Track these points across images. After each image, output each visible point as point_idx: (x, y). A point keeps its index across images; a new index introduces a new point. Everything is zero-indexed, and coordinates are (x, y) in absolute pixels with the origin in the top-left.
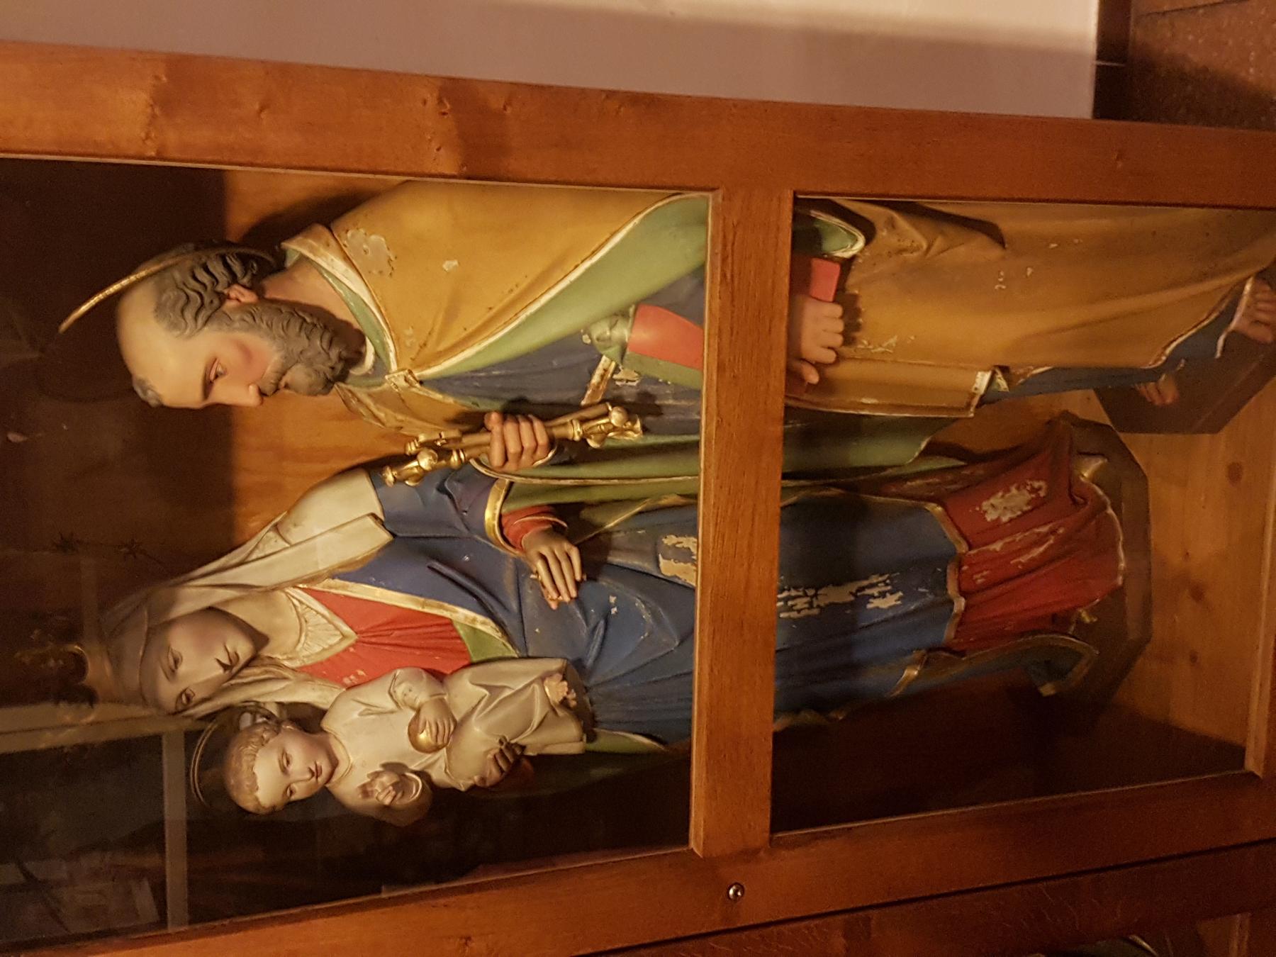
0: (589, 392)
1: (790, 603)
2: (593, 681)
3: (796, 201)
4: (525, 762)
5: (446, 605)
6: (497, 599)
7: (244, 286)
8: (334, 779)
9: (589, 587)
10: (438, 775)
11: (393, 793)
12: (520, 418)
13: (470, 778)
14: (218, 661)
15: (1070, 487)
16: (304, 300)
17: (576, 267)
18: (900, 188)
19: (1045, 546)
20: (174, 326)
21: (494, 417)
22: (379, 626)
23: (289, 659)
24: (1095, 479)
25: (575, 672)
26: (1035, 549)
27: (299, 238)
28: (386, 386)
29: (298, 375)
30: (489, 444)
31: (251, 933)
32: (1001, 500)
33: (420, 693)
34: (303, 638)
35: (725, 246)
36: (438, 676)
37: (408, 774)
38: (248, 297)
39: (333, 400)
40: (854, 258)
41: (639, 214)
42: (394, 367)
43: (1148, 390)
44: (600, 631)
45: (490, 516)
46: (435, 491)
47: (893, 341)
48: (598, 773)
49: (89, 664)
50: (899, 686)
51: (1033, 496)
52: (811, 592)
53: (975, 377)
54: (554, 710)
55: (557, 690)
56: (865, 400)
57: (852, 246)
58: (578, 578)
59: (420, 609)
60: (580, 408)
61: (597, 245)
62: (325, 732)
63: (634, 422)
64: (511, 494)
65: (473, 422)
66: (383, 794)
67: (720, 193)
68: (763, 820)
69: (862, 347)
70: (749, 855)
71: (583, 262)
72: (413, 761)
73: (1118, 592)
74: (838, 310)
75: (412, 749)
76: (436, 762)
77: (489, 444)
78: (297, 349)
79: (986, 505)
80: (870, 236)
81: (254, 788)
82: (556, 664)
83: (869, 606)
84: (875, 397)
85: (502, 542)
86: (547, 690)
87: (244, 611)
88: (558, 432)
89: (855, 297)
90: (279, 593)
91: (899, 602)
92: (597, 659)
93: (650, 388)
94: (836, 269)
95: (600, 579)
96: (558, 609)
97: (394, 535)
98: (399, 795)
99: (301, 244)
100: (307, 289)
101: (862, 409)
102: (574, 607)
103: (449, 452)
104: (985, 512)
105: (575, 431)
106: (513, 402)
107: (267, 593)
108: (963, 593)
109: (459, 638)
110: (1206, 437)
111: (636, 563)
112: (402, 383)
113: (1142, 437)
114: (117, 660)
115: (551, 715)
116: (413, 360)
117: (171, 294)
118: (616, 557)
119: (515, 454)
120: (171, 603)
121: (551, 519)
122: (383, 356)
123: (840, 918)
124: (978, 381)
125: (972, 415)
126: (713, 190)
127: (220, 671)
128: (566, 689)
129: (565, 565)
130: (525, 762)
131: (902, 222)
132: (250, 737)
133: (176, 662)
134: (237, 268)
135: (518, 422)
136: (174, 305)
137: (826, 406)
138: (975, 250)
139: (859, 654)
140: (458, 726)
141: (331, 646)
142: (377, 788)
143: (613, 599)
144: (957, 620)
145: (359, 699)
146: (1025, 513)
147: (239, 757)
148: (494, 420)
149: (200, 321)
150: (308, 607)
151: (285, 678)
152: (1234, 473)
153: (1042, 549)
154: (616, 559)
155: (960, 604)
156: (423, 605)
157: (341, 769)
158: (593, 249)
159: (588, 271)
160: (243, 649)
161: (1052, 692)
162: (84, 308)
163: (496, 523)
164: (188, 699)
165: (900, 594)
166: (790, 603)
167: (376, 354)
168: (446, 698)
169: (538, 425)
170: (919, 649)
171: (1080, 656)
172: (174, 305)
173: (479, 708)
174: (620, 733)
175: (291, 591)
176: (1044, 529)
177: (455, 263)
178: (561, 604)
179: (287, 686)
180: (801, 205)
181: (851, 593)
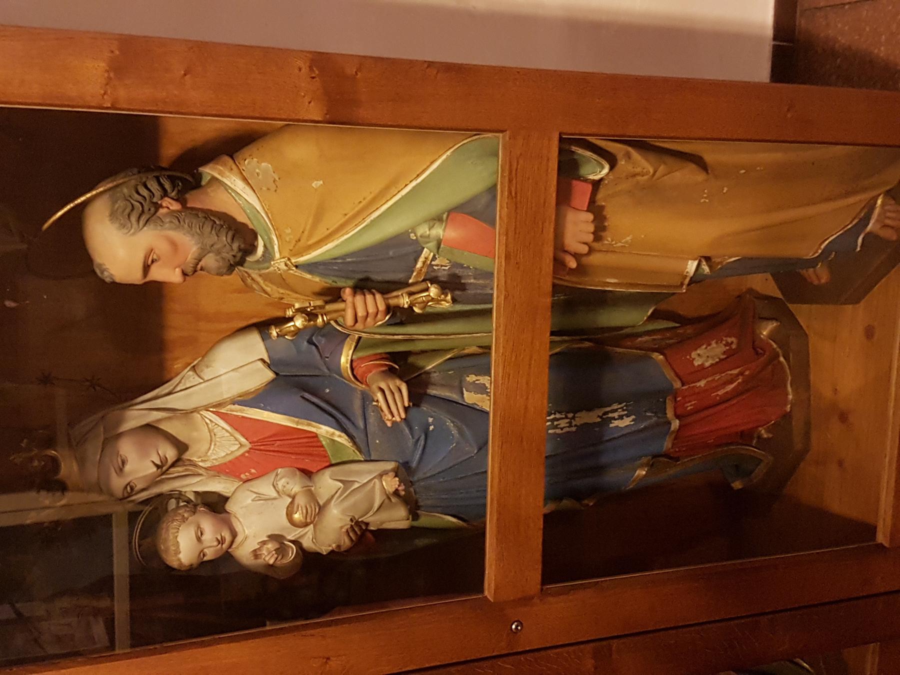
0: (414, 274)
1: (555, 423)
2: (420, 475)
3: (561, 140)
4: (369, 535)
6: (349, 419)
8: (234, 546)
9: (414, 411)
10: (307, 543)
11: (276, 556)
16: (213, 209)
18: (633, 130)
19: (735, 384)
20: (123, 226)
22: (265, 438)
23: (202, 461)
24: (771, 336)
25: (404, 471)
26: (729, 386)
27: (211, 165)
29: (210, 261)
30: (344, 310)
31: (175, 654)
33: (295, 486)
34: (212, 447)
36: (308, 474)
38: (176, 206)
39: (234, 278)
40: (601, 180)
42: (277, 255)
44: (422, 442)
45: (344, 360)
46: (306, 343)
50: (633, 481)
51: (728, 348)
52: (570, 415)
54: (389, 498)
55: (391, 483)
56: (608, 280)
57: (600, 172)
58: (406, 404)
59: (295, 426)
60: (408, 285)
63: (446, 296)
65: (333, 295)
66: (269, 557)
68: (536, 576)
70: (526, 600)
71: (411, 182)
72: (289, 534)
74: (590, 217)
77: (344, 310)
79: (694, 355)
80: (613, 164)
81: (178, 552)
82: (391, 465)
83: (611, 425)
85: (353, 379)
86: (384, 484)
87: (172, 427)
88: (393, 302)
90: (196, 415)
93: (457, 271)
95: (422, 405)
97: (277, 374)
99: (214, 169)
100: (217, 201)
101: (608, 286)
102: (403, 425)
103: (316, 316)
107: (186, 414)
108: (677, 417)
109: (322, 446)
112: (283, 267)
114: (82, 462)
115: (387, 501)
117: (121, 204)
119: (363, 317)
120: (119, 422)
125: (684, 291)
126: (502, 131)
127: (155, 469)
128: (398, 483)
131: (635, 154)
133: (123, 463)
134: (167, 186)
136: (123, 211)
138: (687, 174)
139: (604, 459)
141: (232, 452)
142: (264, 552)
143: (431, 420)
144: (673, 436)
146: (721, 360)
148: (347, 293)
150: (216, 424)
152: (869, 333)
154: (432, 391)
155: (676, 424)
156: (297, 423)
159: (414, 188)
160: (170, 453)
161: (740, 487)
162: (60, 214)
163: (348, 365)
164: (132, 489)
165: (633, 417)
166: (555, 423)
167: (265, 246)
168: (313, 489)
169: (378, 296)
170: (646, 456)
172: (123, 211)
175: (204, 413)
176: (735, 372)
178: (394, 423)
180: (565, 143)
181: (599, 416)
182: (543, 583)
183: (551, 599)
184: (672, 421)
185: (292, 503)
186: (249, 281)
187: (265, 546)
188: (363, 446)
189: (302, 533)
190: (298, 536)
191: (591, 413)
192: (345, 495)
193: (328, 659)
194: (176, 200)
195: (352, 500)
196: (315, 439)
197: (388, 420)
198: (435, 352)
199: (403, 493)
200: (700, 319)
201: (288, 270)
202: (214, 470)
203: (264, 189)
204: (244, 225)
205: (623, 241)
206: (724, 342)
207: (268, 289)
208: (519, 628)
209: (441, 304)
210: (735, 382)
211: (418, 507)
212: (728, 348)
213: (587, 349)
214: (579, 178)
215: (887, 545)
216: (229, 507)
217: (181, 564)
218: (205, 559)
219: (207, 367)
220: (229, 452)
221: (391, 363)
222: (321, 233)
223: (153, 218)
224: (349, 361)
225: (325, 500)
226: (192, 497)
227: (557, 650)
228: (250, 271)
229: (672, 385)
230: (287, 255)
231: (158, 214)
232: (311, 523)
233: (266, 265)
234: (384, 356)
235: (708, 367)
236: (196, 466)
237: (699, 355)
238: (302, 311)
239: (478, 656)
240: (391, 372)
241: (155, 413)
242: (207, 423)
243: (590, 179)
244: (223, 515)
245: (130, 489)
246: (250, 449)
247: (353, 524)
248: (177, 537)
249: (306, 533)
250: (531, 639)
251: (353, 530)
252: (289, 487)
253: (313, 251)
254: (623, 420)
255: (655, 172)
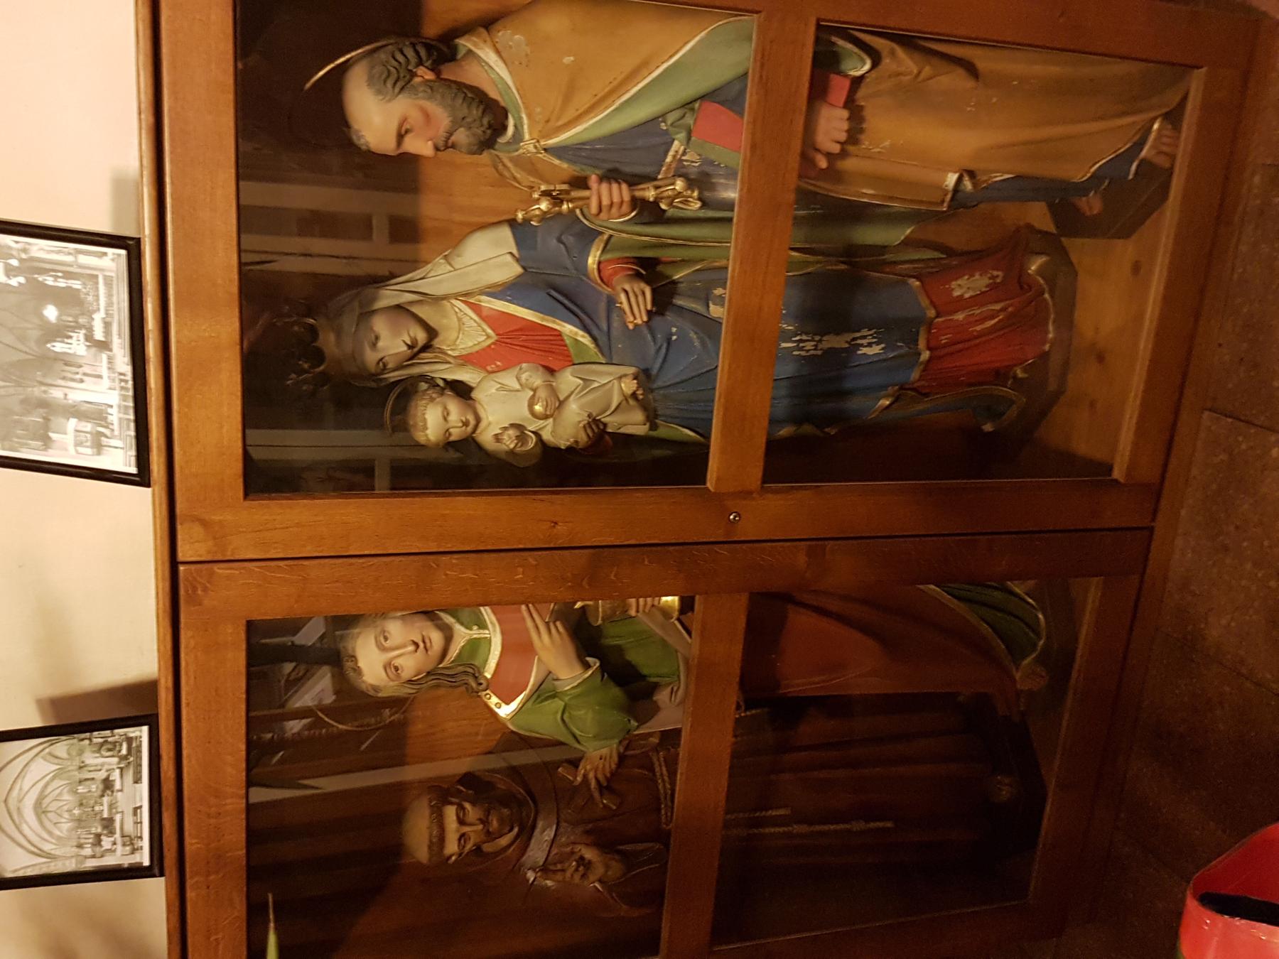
0: (664, 169)
1: (801, 345)
2: (659, 383)
3: (819, 27)
4: (607, 437)
5: (557, 321)
6: (592, 319)
7: (427, 67)
8: (478, 431)
9: (657, 320)
10: (546, 436)
11: (516, 441)
12: (613, 181)
13: (568, 440)
14: (404, 342)
15: (1020, 276)
16: (468, 82)
17: (658, 67)
18: (896, 22)
19: (996, 320)
20: (379, 92)
21: (594, 177)
22: (512, 331)
23: (452, 350)
24: (1040, 271)
25: (645, 376)
26: (988, 322)
27: (467, 37)
28: (521, 151)
29: (461, 136)
30: (588, 198)
31: (417, 499)
32: (965, 282)
33: (537, 380)
34: (461, 335)
35: (763, 55)
36: (551, 371)
37: (526, 432)
38: (430, 76)
39: (485, 157)
40: (862, 77)
41: (705, 30)
42: (527, 137)
43: (1082, 203)
44: (663, 350)
45: (592, 261)
46: (555, 241)
47: (887, 143)
48: (658, 452)
49: (320, 333)
50: (874, 412)
51: (991, 281)
52: (817, 338)
53: (946, 176)
54: (626, 400)
55: (629, 386)
56: (864, 191)
57: (862, 67)
58: (649, 307)
59: (540, 322)
60: (656, 179)
61: (674, 51)
62: (474, 400)
63: (693, 192)
64: (608, 247)
65: (580, 183)
66: (509, 442)
67: (763, 15)
68: (756, 472)
69: (864, 146)
70: (746, 494)
71: (663, 63)
72: (531, 425)
73: (1045, 356)
74: (845, 114)
75: (530, 416)
76: (548, 425)
77: (588, 198)
78: (461, 116)
79: (954, 285)
80: (875, 64)
81: (425, 428)
82: (631, 370)
83: (859, 352)
84: (872, 189)
85: (599, 281)
86: (623, 385)
87: (422, 312)
88: (638, 194)
89: (861, 108)
90: (445, 302)
91: (881, 352)
92: (661, 368)
93: (708, 169)
94: (847, 83)
95: (668, 313)
96: (634, 329)
97: (524, 268)
98: (520, 444)
99: (468, 40)
100: (471, 74)
101: (863, 198)
102: (645, 331)
103: (562, 202)
104: (953, 289)
105: (650, 194)
106: (610, 171)
107: (437, 300)
108: (929, 348)
109: (565, 346)
110: (1120, 242)
111: (693, 305)
112: (531, 148)
113: (1079, 241)
114: (339, 334)
115: (624, 402)
116: (540, 131)
117: (378, 69)
118: (681, 300)
119: (608, 205)
120: (374, 299)
121: (634, 267)
122: (519, 128)
123: (803, 543)
124: (949, 179)
125: (945, 209)
126: (757, 12)
127: (405, 348)
128: (636, 385)
129: (640, 299)
130: (607, 437)
131: (900, 52)
132: (424, 395)
133: (377, 338)
134: (423, 53)
135: (610, 184)
136: (380, 76)
137: (837, 193)
138: (954, 80)
139: (849, 384)
140: (562, 403)
141: (479, 343)
142: (505, 437)
143: (674, 330)
144: (922, 367)
145: (497, 380)
146: (983, 293)
147: (416, 406)
148: (593, 181)
149: (397, 90)
150: (465, 314)
151: (449, 363)
152: (1136, 268)
153: (993, 322)
154: (679, 301)
155: (926, 355)
156: (543, 319)
157: (483, 425)
158: (670, 54)
159: (666, 70)
160: (421, 336)
161: (991, 430)
162: (321, 73)
163: (595, 266)
164: (385, 365)
165: (883, 345)
166: (801, 345)
167: (515, 126)
168: (554, 384)
169: (624, 186)
170: (894, 385)
171: (1013, 402)
172: (380, 76)
173: (576, 391)
174: (672, 425)
175: (454, 301)
176: (998, 307)
177: (572, 58)
178: (636, 325)
179: (450, 367)
180: (824, 31)
181: (847, 342)
182: (764, 482)
183: (770, 496)
184: (922, 352)
185: (533, 396)
186: (500, 167)
187: (506, 432)
188: (606, 350)
189: (544, 425)
190: (537, 428)
191: (838, 338)
192: (585, 392)
193: (556, 523)
194: (432, 70)
195: (591, 397)
196: (560, 337)
197: (630, 322)
198: (684, 262)
199: (641, 397)
200: (969, 253)
201: (537, 153)
202: (462, 360)
203: (517, 63)
204: (495, 102)
205: (881, 146)
206: (989, 275)
207: (518, 176)
208: (737, 518)
209: (690, 206)
210: (996, 318)
211: (656, 416)
212: (991, 281)
213: (843, 270)
214: (839, 73)
215: (1122, 480)
216: (474, 395)
217: (428, 440)
218: (452, 439)
219: (459, 256)
220: (476, 343)
221: (638, 268)
222: (571, 113)
223: (408, 86)
224: (596, 262)
225: (566, 394)
226: (441, 383)
227: (774, 544)
228: (501, 155)
229: (925, 313)
230: (535, 136)
231: (412, 83)
232: (551, 416)
233: (516, 147)
234: (632, 261)
235: (967, 299)
236: (446, 354)
237: (959, 285)
238: (546, 194)
239: (696, 539)
240: (638, 276)
241: (407, 294)
242: (456, 313)
243: (850, 75)
244: (470, 402)
245: (382, 364)
246: (497, 341)
247: (590, 420)
248: (424, 414)
249: (548, 425)
250: (749, 528)
251: (590, 427)
252: (531, 380)
253: (562, 134)
254: (872, 349)
255: (919, 73)
